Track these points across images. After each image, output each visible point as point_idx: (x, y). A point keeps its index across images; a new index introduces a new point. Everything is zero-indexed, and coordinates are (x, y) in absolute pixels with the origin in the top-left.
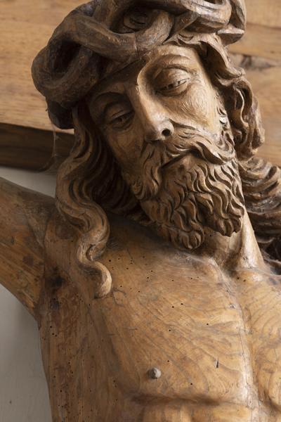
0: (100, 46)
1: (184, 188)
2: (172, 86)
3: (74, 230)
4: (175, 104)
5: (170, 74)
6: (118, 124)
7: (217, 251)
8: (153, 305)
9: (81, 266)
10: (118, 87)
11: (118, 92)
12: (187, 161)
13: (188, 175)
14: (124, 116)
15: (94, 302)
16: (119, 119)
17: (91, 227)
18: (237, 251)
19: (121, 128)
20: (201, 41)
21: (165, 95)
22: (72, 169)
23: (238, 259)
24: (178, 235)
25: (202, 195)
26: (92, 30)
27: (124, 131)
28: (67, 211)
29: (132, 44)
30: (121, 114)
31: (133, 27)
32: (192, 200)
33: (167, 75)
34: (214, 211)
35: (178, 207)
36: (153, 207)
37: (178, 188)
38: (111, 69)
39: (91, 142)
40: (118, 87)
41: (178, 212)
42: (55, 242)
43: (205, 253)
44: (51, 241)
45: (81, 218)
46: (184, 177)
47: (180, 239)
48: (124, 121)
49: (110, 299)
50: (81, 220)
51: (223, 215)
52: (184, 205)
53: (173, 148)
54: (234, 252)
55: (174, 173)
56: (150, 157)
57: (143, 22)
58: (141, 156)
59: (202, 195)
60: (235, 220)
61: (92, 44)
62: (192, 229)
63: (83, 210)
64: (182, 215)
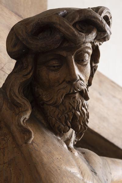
0: (70, 34)
1: (72, 106)
2: (83, 60)
3: (16, 107)
4: (82, 69)
5: (85, 55)
6: (52, 68)
7: (63, 136)
8: (50, 155)
9: (20, 126)
10: (64, 53)
11: (64, 55)
12: (77, 95)
13: (76, 101)
14: (57, 66)
15: (24, 145)
16: (54, 67)
17: (26, 110)
18: (69, 139)
19: (53, 70)
20: (97, 45)
21: (78, 63)
22: (23, 80)
23: (69, 142)
24: (60, 126)
25: (78, 112)
26: (68, 26)
27: (53, 72)
28: (15, 98)
29: (83, 38)
30: (55, 65)
31: (80, 30)
32: (73, 112)
33: (84, 55)
34: (79, 120)
35: (65, 114)
36: (53, 109)
37: (70, 105)
38: (67, 45)
39: (33, 69)
40: (64, 53)
41: (65, 116)
42: (7, 110)
43: (58, 135)
44: (5, 109)
45: (22, 103)
46: (74, 102)
47: (60, 128)
48: (56, 68)
49: (31, 146)
50: (22, 105)
51: (82, 124)
52: (68, 113)
53: (76, 88)
54: (68, 138)
55: (70, 99)
56: (64, 88)
57: (84, 29)
58: (58, 86)
59: (78, 112)
60: (85, 127)
61: (66, 32)
62: (67, 125)
63: (23, 100)
64: (66, 117)
